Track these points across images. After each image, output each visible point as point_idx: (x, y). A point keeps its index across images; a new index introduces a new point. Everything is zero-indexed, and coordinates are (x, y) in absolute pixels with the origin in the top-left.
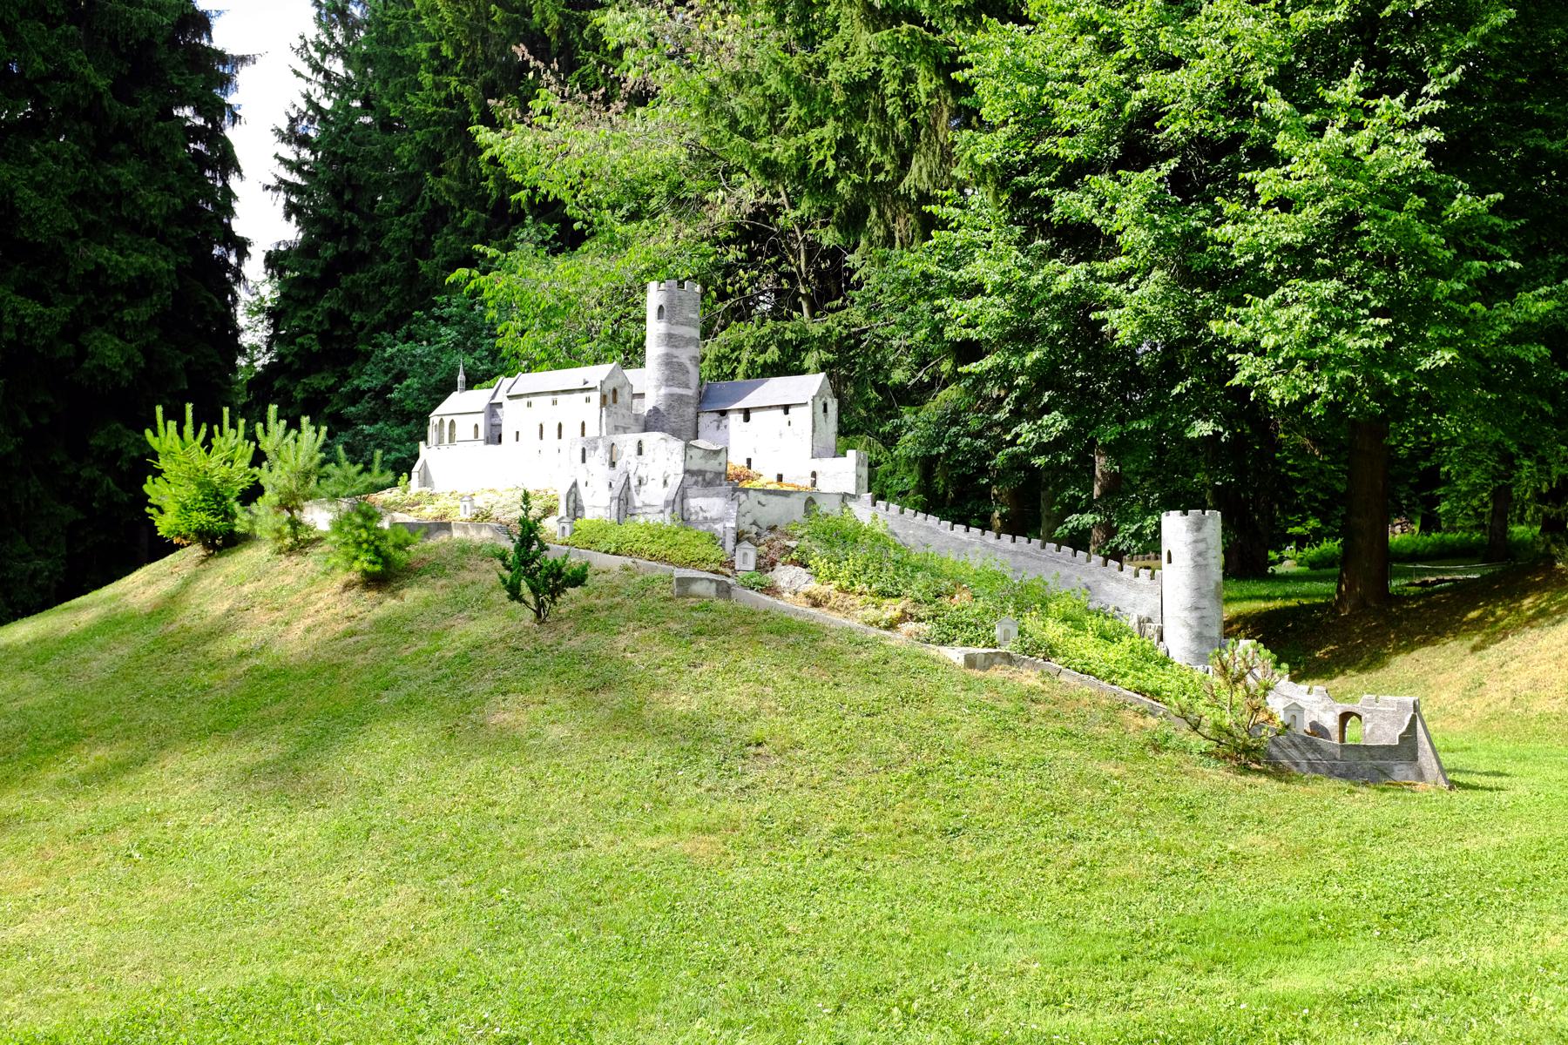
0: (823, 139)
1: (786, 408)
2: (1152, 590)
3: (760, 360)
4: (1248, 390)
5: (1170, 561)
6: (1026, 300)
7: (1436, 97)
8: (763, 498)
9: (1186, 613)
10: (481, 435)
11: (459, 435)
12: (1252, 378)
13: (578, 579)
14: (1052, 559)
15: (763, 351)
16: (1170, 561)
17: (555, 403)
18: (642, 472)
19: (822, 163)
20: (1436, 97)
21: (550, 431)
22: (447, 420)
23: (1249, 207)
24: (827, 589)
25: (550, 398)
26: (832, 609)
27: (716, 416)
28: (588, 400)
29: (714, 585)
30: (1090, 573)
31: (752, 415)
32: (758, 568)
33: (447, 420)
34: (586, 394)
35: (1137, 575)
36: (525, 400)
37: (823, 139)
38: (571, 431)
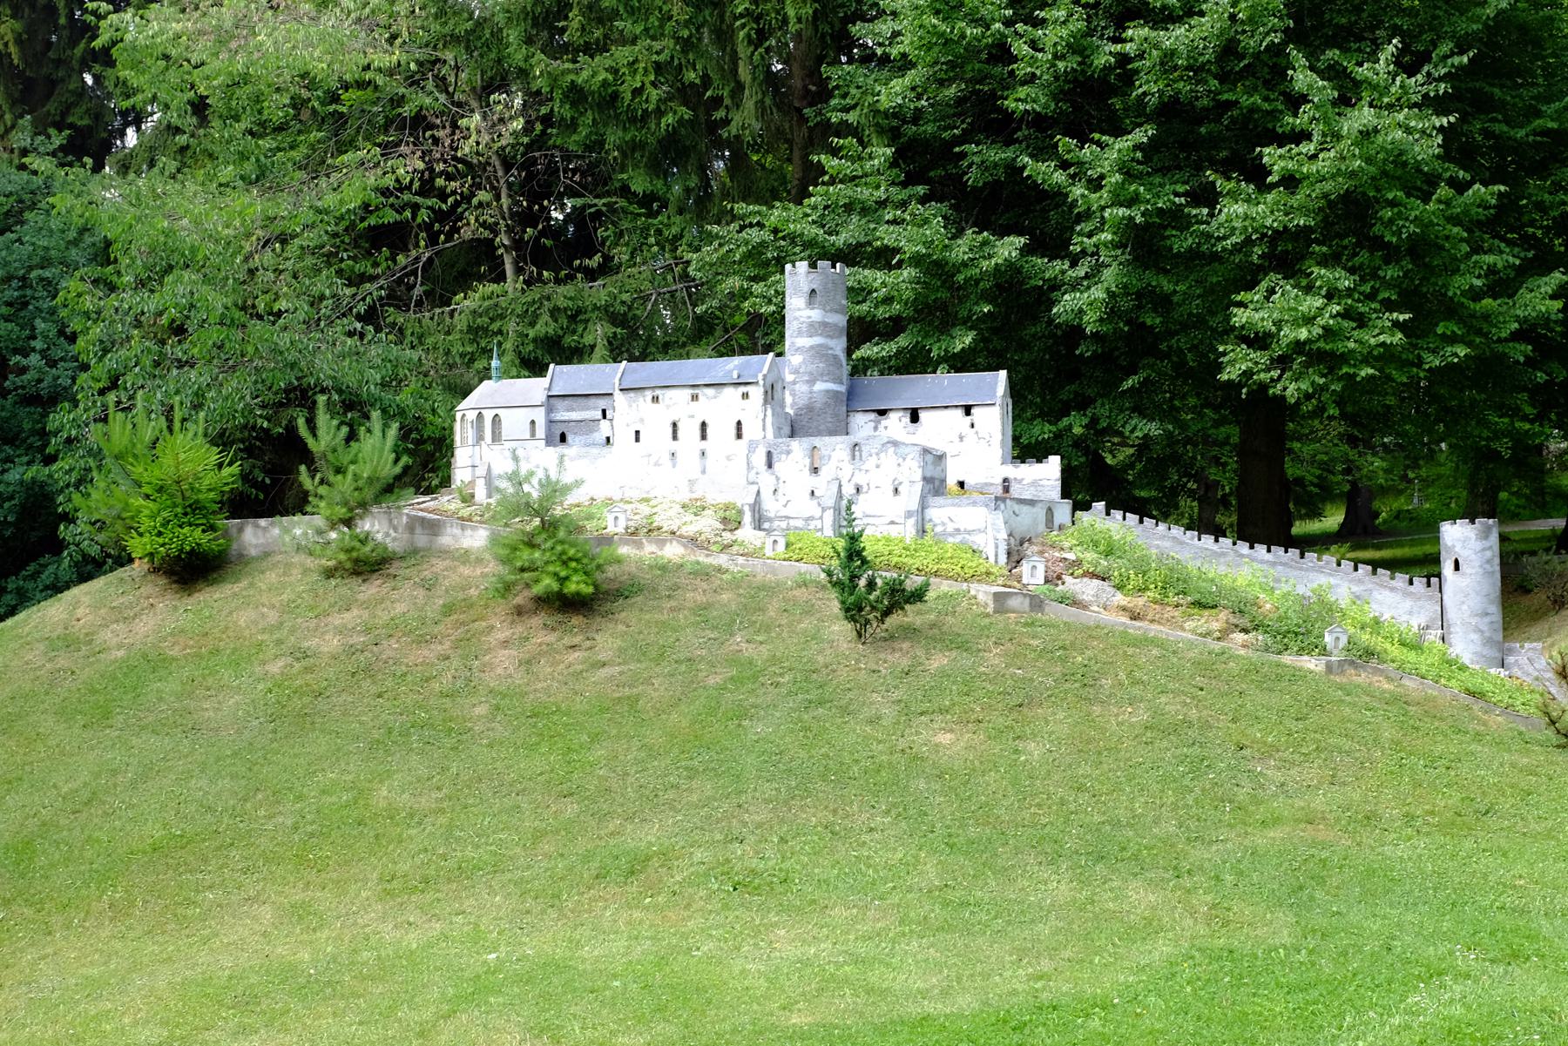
0: (636, 61)
1: (968, 410)
2: (1431, 598)
3: (532, 333)
4: (1240, 385)
5: (1457, 567)
6: (935, 269)
7: (1440, 79)
8: (1016, 507)
9: (1474, 621)
10: (541, 432)
11: (506, 431)
12: (1248, 374)
13: (519, 612)
14: (1313, 569)
15: (532, 324)
16: (1457, 567)
17: (695, 398)
18: (860, 479)
19: (637, 92)
20: (1440, 79)
21: (689, 431)
22: (488, 416)
23: (1014, 159)
24: (1141, 601)
25: (690, 391)
26: (1152, 621)
27: (873, 416)
28: (745, 396)
29: (1027, 600)
30: (1360, 581)
31: (923, 415)
32: (1047, 581)
33: (488, 416)
34: (743, 389)
35: (1411, 583)
36: (649, 394)
37: (636, 61)
38: (721, 431)
